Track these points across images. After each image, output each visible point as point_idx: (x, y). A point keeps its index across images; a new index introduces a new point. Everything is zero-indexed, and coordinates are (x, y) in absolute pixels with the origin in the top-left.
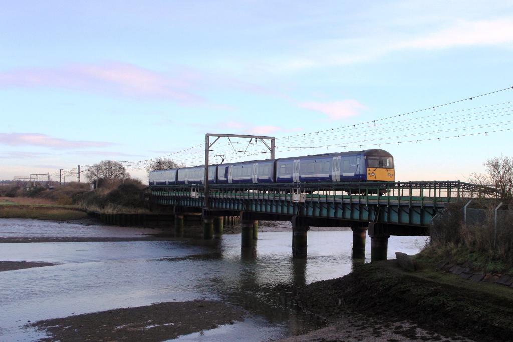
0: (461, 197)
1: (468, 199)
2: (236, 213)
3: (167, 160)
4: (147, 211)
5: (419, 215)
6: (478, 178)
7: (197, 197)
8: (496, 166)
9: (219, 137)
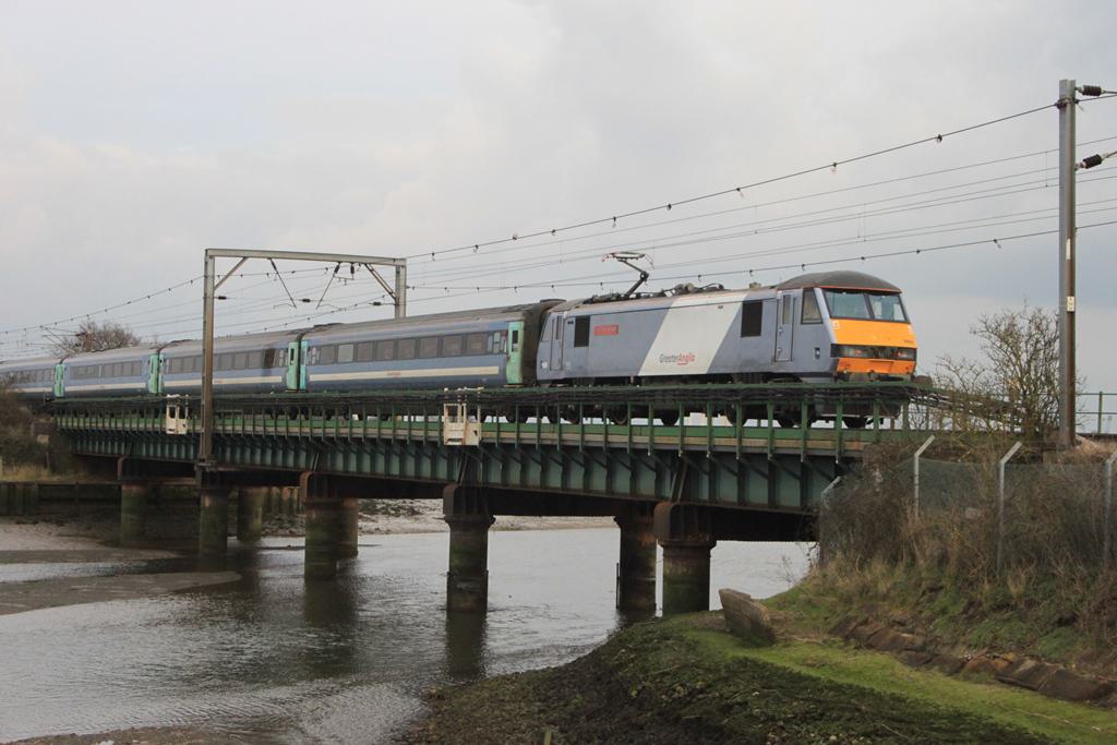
0: (912, 427)
1: (927, 433)
2: (291, 478)
3: (112, 327)
4: (45, 476)
5: (735, 478)
6: (956, 372)
7: (183, 431)
8: (1008, 337)
9: (245, 258)
